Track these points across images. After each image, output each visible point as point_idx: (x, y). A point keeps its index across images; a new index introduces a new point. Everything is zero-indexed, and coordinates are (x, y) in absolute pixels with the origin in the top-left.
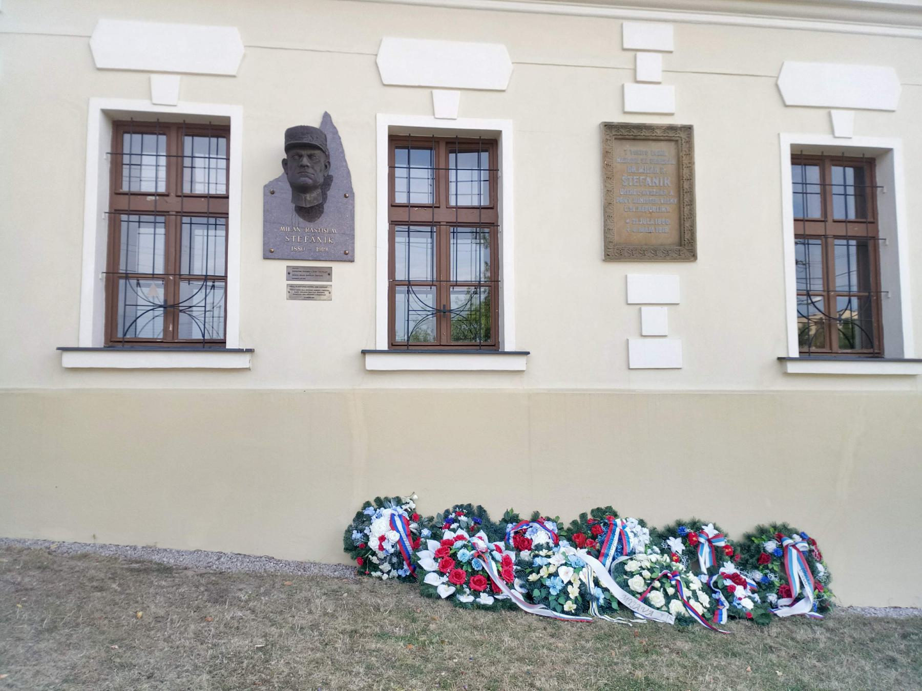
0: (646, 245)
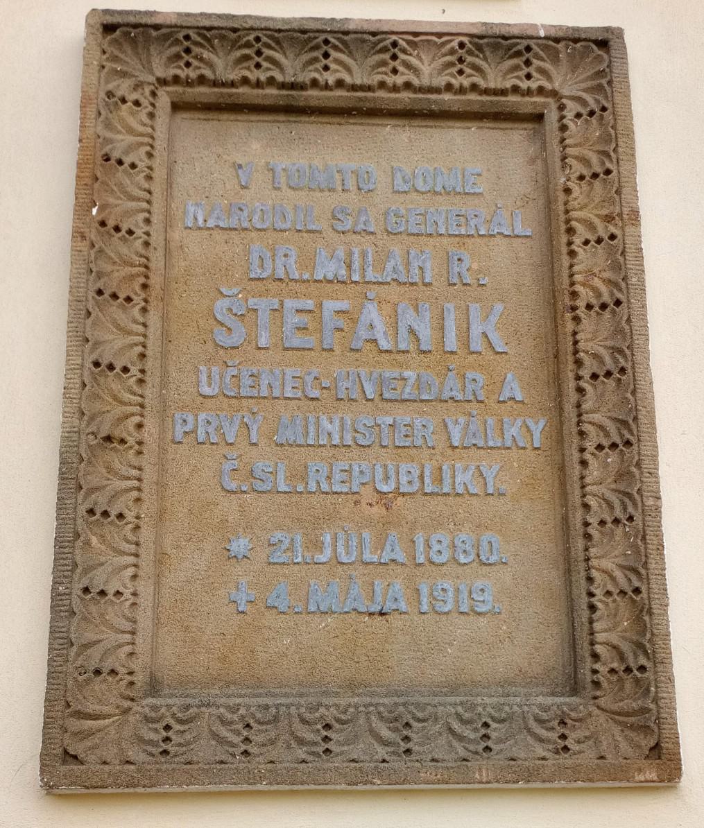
0: (352, 686)
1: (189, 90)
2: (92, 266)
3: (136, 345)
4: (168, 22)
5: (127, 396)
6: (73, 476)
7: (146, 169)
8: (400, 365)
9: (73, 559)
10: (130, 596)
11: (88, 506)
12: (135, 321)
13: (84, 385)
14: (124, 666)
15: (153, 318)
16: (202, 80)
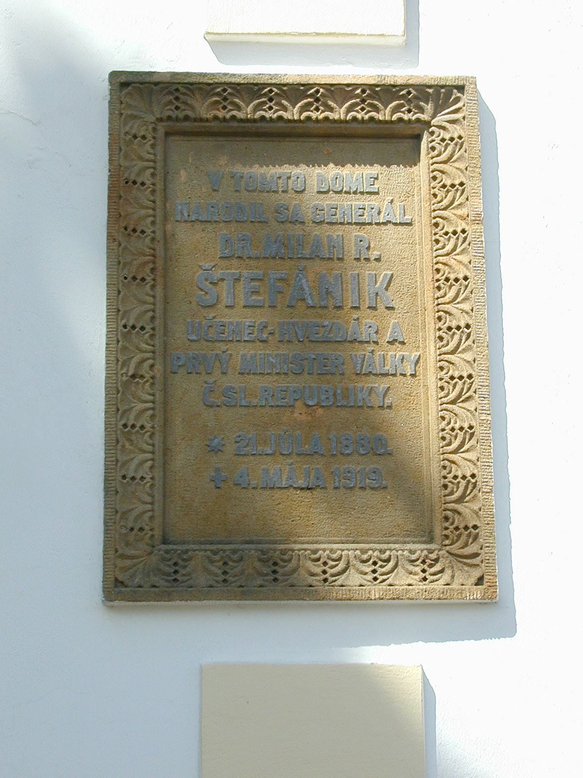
1: (178, 124)
2: (121, 259)
3: (148, 311)
4: (165, 81)
5: (144, 346)
6: (114, 403)
7: (151, 186)
8: (321, 316)
9: (116, 457)
10: (150, 480)
11: (123, 422)
12: (148, 295)
13: (118, 341)
14: (147, 525)
15: (159, 289)
16: (187, 118)
